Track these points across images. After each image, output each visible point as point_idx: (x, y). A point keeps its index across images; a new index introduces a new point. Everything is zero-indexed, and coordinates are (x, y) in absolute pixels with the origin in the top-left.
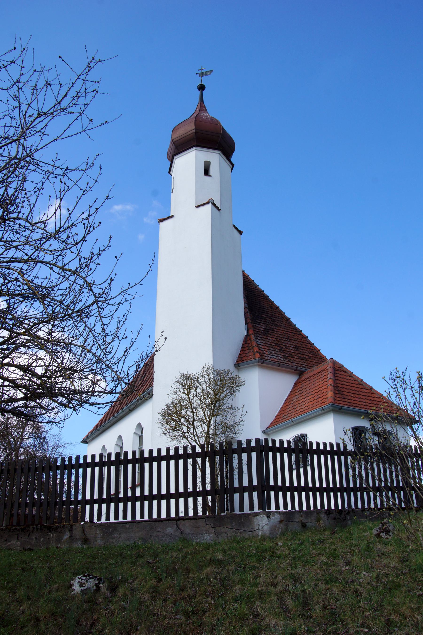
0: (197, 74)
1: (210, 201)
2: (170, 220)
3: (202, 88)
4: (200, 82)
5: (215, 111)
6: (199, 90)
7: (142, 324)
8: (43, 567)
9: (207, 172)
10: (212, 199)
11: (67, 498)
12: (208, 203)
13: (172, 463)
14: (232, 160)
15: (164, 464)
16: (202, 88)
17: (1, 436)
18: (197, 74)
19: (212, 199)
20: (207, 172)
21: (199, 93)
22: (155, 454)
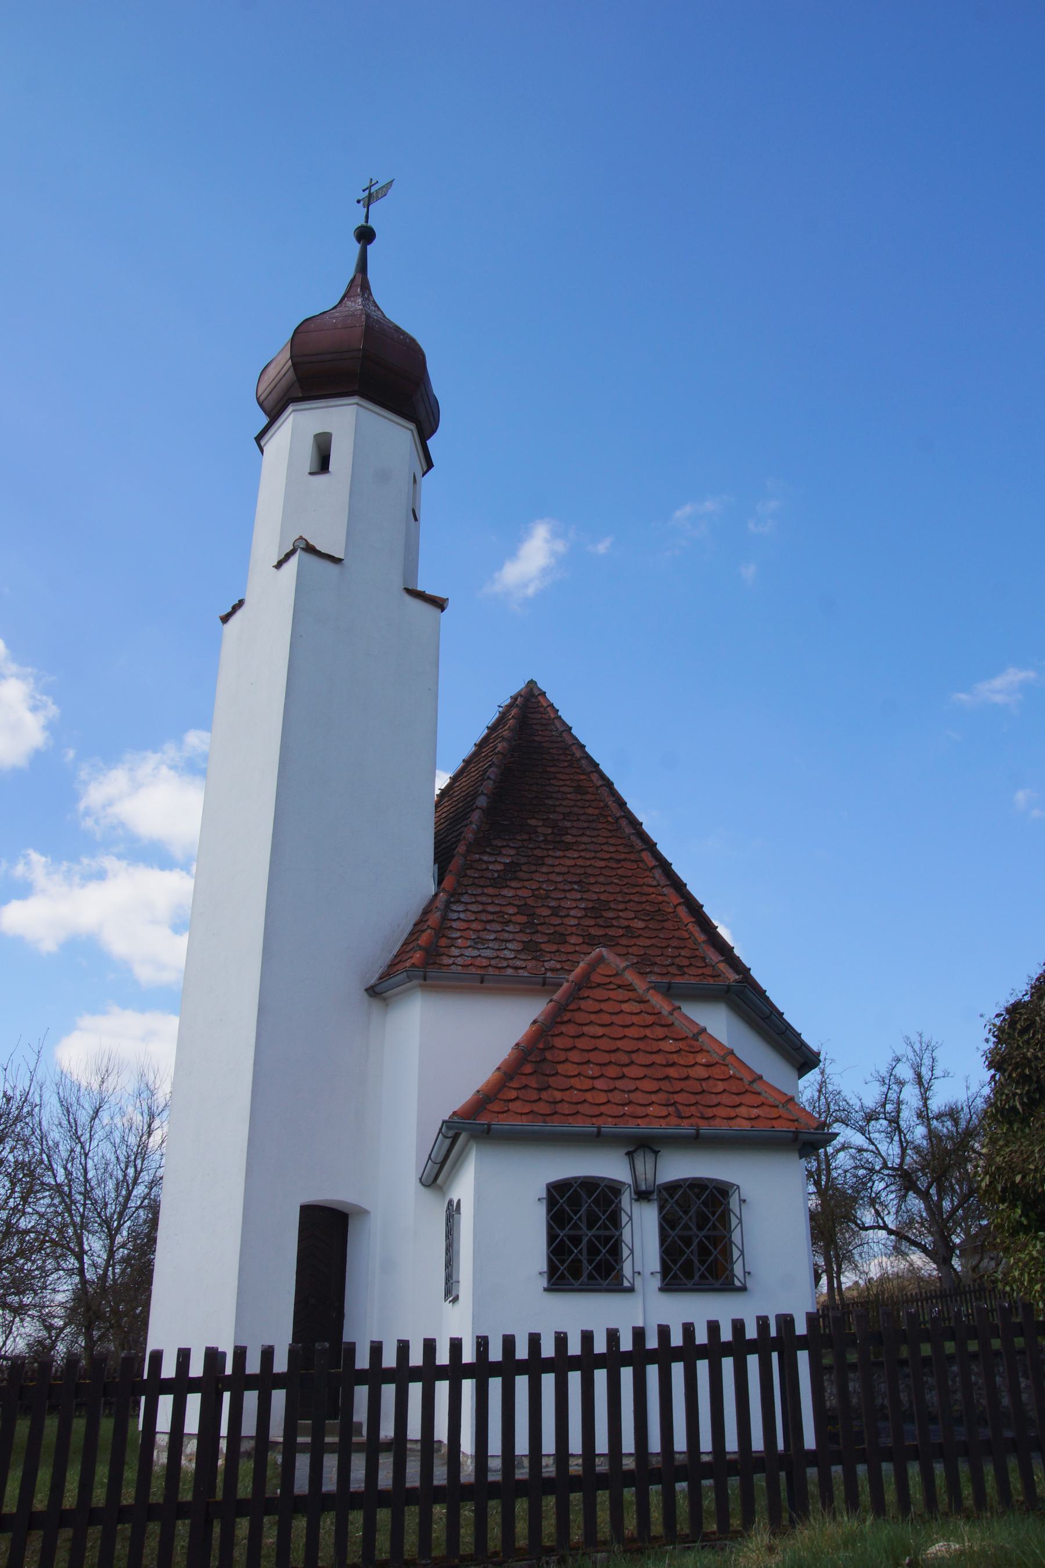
0: (359, 202)
1: (297, 544)
2: (239, 614)
3: (366, 235)
4: (364, 219)
5: (399, 305)
6: (359, 240)
7: (982, 1016)
8: (846, 1546)
9: (323, 464)
10: (301, 538)
11: (137, 1498)
12: (292, 552)
13: (548, 1381)
14: (430, 443)
15: (548, 1381)
16: (366, 235)
17: (2, 1287)
18: (359, 202)
19: (301, 538)
20: (323, 464)
21: (357, 247)
22: (600, 1347)
